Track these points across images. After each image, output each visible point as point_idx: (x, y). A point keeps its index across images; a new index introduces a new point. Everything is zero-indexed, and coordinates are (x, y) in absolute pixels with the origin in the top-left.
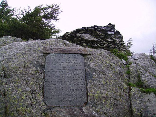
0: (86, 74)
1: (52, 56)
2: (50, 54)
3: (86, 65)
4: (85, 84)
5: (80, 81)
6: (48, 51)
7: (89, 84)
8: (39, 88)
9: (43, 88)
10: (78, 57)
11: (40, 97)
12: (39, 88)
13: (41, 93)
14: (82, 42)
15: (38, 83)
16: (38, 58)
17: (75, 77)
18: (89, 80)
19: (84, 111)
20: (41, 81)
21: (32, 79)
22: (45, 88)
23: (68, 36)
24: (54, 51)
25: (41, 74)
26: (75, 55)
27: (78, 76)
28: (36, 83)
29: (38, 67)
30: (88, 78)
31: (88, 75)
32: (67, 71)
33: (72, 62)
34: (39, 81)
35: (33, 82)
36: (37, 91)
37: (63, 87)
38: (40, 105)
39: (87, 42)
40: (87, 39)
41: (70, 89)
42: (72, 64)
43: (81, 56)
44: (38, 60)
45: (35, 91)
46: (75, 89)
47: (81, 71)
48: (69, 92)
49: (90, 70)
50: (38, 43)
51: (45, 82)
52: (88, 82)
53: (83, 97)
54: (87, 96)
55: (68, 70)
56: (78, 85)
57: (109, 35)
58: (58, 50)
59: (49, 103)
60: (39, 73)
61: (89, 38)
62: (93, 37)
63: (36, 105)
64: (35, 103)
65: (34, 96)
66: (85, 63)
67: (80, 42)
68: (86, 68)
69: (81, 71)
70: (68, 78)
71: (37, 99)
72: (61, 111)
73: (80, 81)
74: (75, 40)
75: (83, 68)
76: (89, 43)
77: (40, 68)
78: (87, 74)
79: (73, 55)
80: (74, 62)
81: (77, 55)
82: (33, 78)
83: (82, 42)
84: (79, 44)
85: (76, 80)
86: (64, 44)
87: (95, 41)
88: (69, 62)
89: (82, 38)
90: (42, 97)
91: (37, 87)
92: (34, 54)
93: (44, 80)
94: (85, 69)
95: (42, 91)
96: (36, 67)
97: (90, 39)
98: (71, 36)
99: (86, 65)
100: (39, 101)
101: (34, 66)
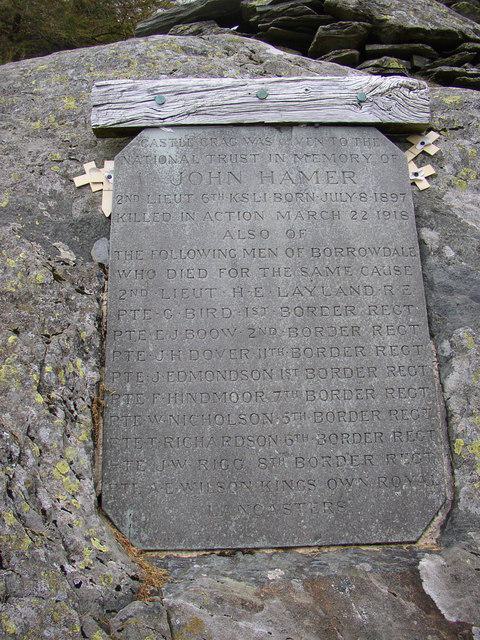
0: (429, 284)
1: (161, 151)
2: (144, 134)
3: (426, 211)
4: (432, 365)
5: (389, 340)
6: (129, 115)
7: (460, 366)
8: (60, 413)
9: (98, 408)
10: (358, 150)
11: (73, 484)
12: (60, 413)
13: (77, 451)
14: (369, 48)
15: (56, 371)
16: (56, 168)
17: (350, 310)
18: (461, 332)
19: (434, 597)
20: (81, 347)
21: (12, 338)
22: (116, 408)
23: (278, 14)
24: (169, 110)
25: (81, 291)
26: (339, 133)
27: (370, 300)
28: (42, 365)
29: (55, 236)
30: (445, 311)
31: (449, 290)
32: (281, 261)
33: (317, 188)
34: (64, 352)
35: (20, 360)
36: (44, 433)
37: (258, 395)
38: (72, 553)
39: (405, 46)
40: (411, 24)
41: (310, 408)
42: (315, 207)
43: (386, 146)
44: (58, 187)
45: (31, 436)
46: (351, 404)
47: (387, 263)
48: (302, 437)
49: (459, 253)
50: (154, 43)
51: (109, 361)
52: (446, 344)
53: (417, 468)
54: (328, 546)
55: (290, 251)
56: (372, 371)
57: (355, 49)
58: (208, 101)
59: (145, 525)
60: (67, 287)
61: (436, 24)
62: (445, 10)
63: (34, 559)
64: (31, 548)
65: (22, 476)
66: (414, 196)
67: (361, 48)
68: (429, 235)
69: (387, 263)
70: (285, 323)
71: (47, 504)
72: (243, 603)
73: (389, 340)
74: (321, 39)
75: (400, 231)
76: (421, 53)
77: (72, 246)
78: (439, 277)
79: (326, 132)
80: (330, 189)
81: (355, 133)
82: (16, 332)
83: (369, 48)
84: (353, 63)
85: (355, 330)
86: (245, 59)
87: (469, 40)
88: (292, 188)
89: (369, 18)
90: (88, 484)
91: (50, 402)
92: (34, 146)
93: (100, 346)
94: (422, 242)
95: (84, 435)
96: (43, 242)
97: (429, 27)
98: (295, 14)
99: (426, 211)
100: (62, 518)
101: (26, 234)
